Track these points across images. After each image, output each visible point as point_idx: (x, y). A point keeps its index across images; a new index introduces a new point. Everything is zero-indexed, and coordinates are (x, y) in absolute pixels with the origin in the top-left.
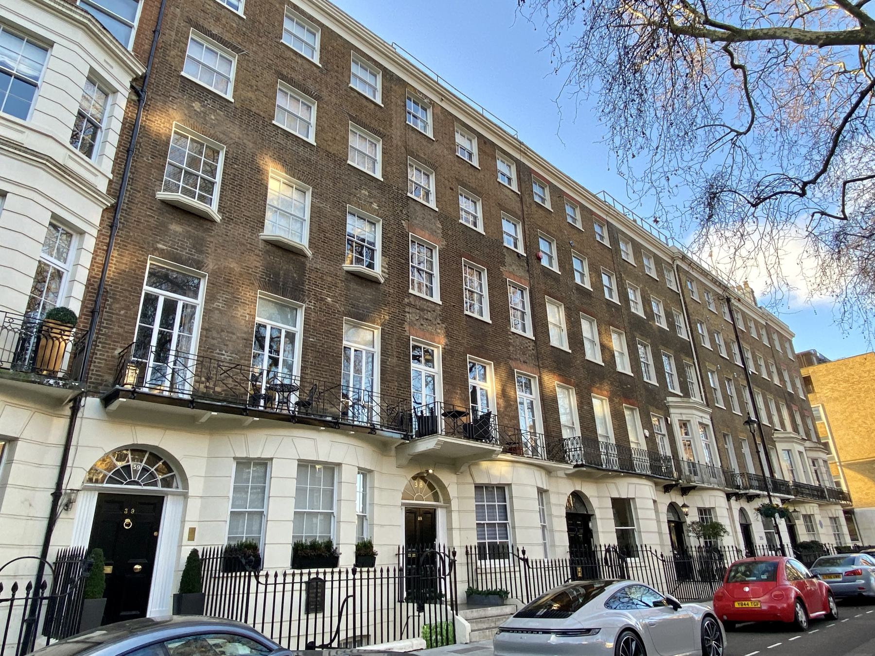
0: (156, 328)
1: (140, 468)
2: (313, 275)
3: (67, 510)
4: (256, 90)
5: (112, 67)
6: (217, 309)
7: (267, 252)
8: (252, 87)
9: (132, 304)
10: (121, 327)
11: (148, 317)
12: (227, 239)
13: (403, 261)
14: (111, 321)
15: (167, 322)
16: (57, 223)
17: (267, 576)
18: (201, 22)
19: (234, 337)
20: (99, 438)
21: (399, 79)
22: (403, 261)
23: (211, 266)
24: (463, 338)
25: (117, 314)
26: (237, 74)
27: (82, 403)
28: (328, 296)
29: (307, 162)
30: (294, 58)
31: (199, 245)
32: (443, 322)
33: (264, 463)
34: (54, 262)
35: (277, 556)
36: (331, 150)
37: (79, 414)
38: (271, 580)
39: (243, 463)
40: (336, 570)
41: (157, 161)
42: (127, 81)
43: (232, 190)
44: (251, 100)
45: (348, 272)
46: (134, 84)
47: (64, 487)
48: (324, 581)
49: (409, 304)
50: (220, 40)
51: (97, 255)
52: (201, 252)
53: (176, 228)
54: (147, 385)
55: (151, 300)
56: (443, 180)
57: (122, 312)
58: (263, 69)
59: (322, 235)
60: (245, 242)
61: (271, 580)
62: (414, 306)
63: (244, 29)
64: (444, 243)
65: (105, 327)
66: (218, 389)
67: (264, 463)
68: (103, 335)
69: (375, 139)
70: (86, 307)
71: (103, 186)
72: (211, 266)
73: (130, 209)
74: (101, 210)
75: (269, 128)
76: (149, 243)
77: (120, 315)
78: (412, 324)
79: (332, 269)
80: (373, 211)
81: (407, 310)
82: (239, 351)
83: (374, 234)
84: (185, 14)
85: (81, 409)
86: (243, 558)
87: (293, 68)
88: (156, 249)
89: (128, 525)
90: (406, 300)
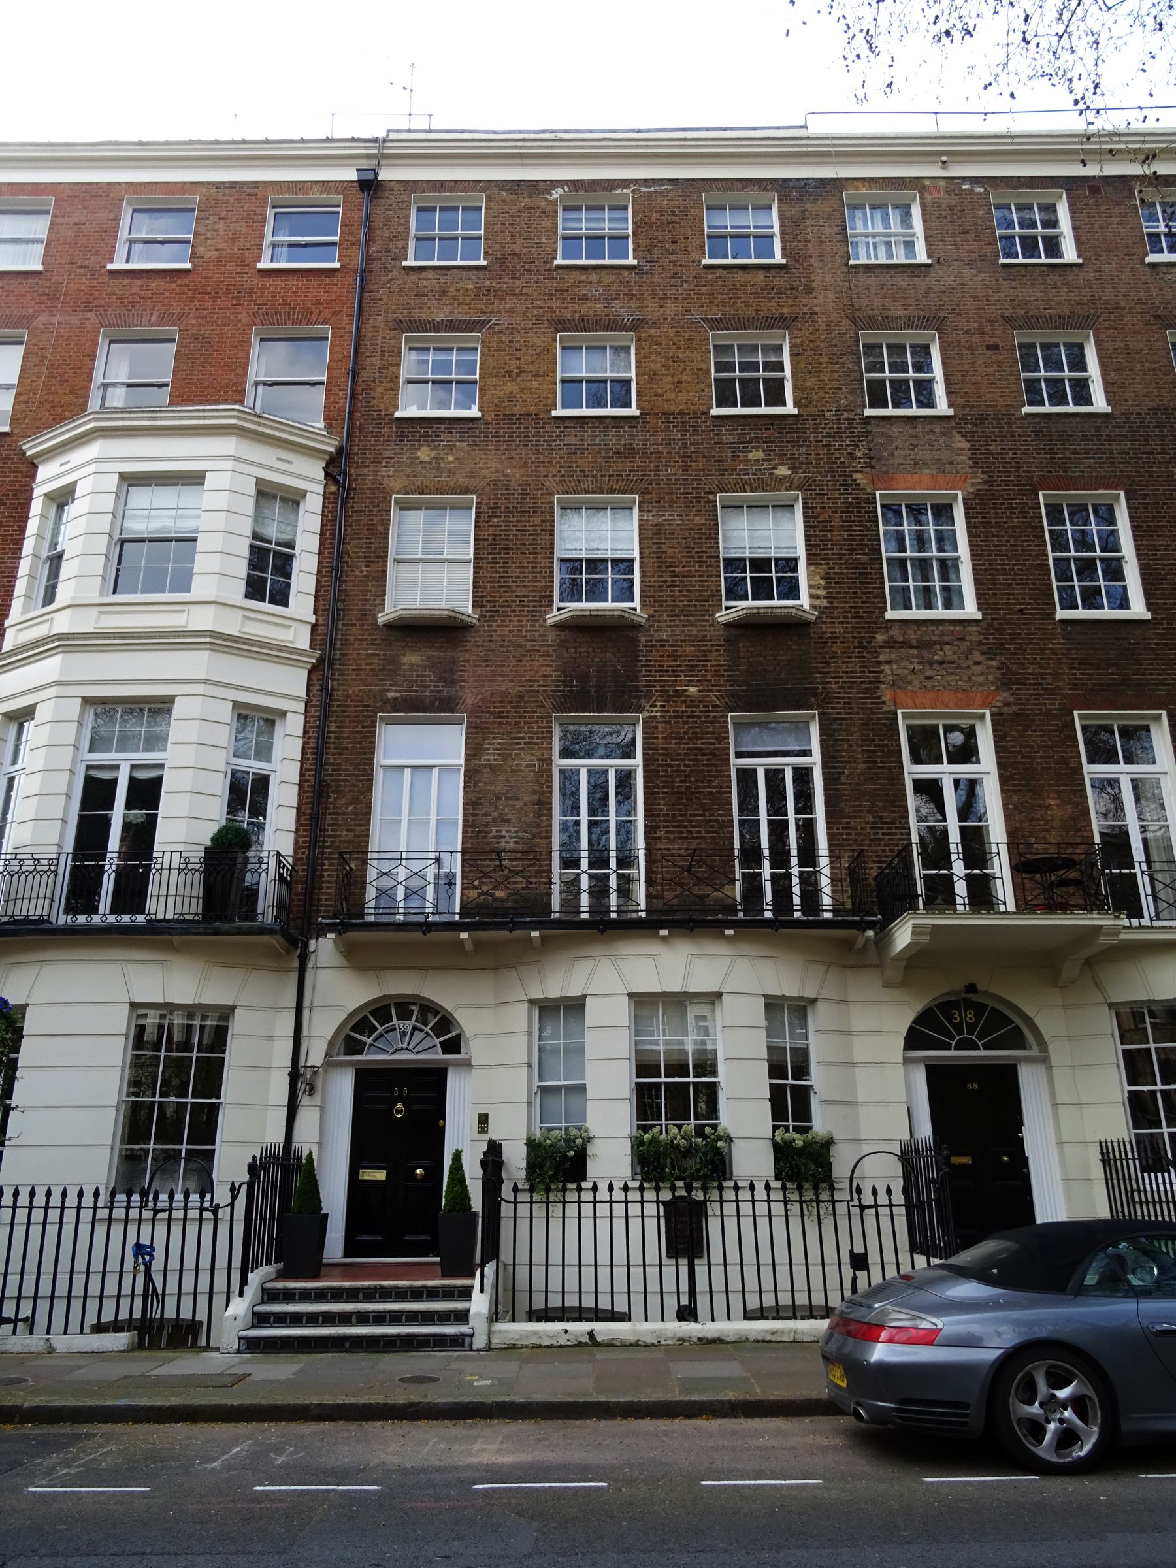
0: (763, 817)
1: (409, 1029)
2: (655, 655)
3: (310, 1095)
4: (518, 375)
5: (290, 462)
6: (485, 766)
7: (563, 644)
8: (509, 373)
9: (362, 793)
10: (351, 831)
11: (748, 804)
12: (493, 646)
13: (865, 558)
14: (339, 825)
15: (598, 804)
16: (244, 714)
17: (595, 1188)
18: (416, 314)
19: (520, 803)
20: (339, 989)
21: (823, 181)
22: (865, 558)
23: (470, 701)
24: (1057, 676)
25: (343, 814)
26: (924, 221)
27: (312, 949)
28: (690, 683)
29: (627, 452)
30: (583, 278)
31: (448, 674)
32: (989, 655)
33: (575, 1006)
34: (253, 765)
35: (611, 1159)
36: (673, 408)
37: (311, 964)
38: (603, 1194)
39: (547, 1009)
40: (729, 1184)
41: (374, 567)
42: (316, 470)
43: (494, 563)
44: (510, 397)
45: (728, 625)
46: (330, 470)
47: (302, 1063)
48: (913, 1250)
49: (890, 644)
50: (452, 326)
51: (310, 738)
52: (452, 683)
53: (411, 659)
54: (401, 910)
55: (569, 777)
56: (964, 338)
57: (350, 809)
58: (528, 330)
59: (666, 576)
60: (521, 640)
61: (603, 1194)
62: (905, 644)
63: (488, 283)
64: (980, 477)
65: (330, 836)
66: (500, 894)
67: (575, 1006)
68: (328, 847)
69: (770, 337)
70: (305, 814)
71: (303, 640)
72: (470, 701)
73: (345, 655)
74: (306, 672)
75: (547, 427)
76: (375, 696)
77: (348, 814)
78: (899, 683)
79: (694, 631)
80: (780, 483)
81: (882, 657)
82: (529, 826)
83: (781, 534)
84: (391, 317)
85: (313, 956)
86: (560, 1166)
87: (584, 299)
88: (387, 701)
89: (398, 1112)
90: (880, 638)
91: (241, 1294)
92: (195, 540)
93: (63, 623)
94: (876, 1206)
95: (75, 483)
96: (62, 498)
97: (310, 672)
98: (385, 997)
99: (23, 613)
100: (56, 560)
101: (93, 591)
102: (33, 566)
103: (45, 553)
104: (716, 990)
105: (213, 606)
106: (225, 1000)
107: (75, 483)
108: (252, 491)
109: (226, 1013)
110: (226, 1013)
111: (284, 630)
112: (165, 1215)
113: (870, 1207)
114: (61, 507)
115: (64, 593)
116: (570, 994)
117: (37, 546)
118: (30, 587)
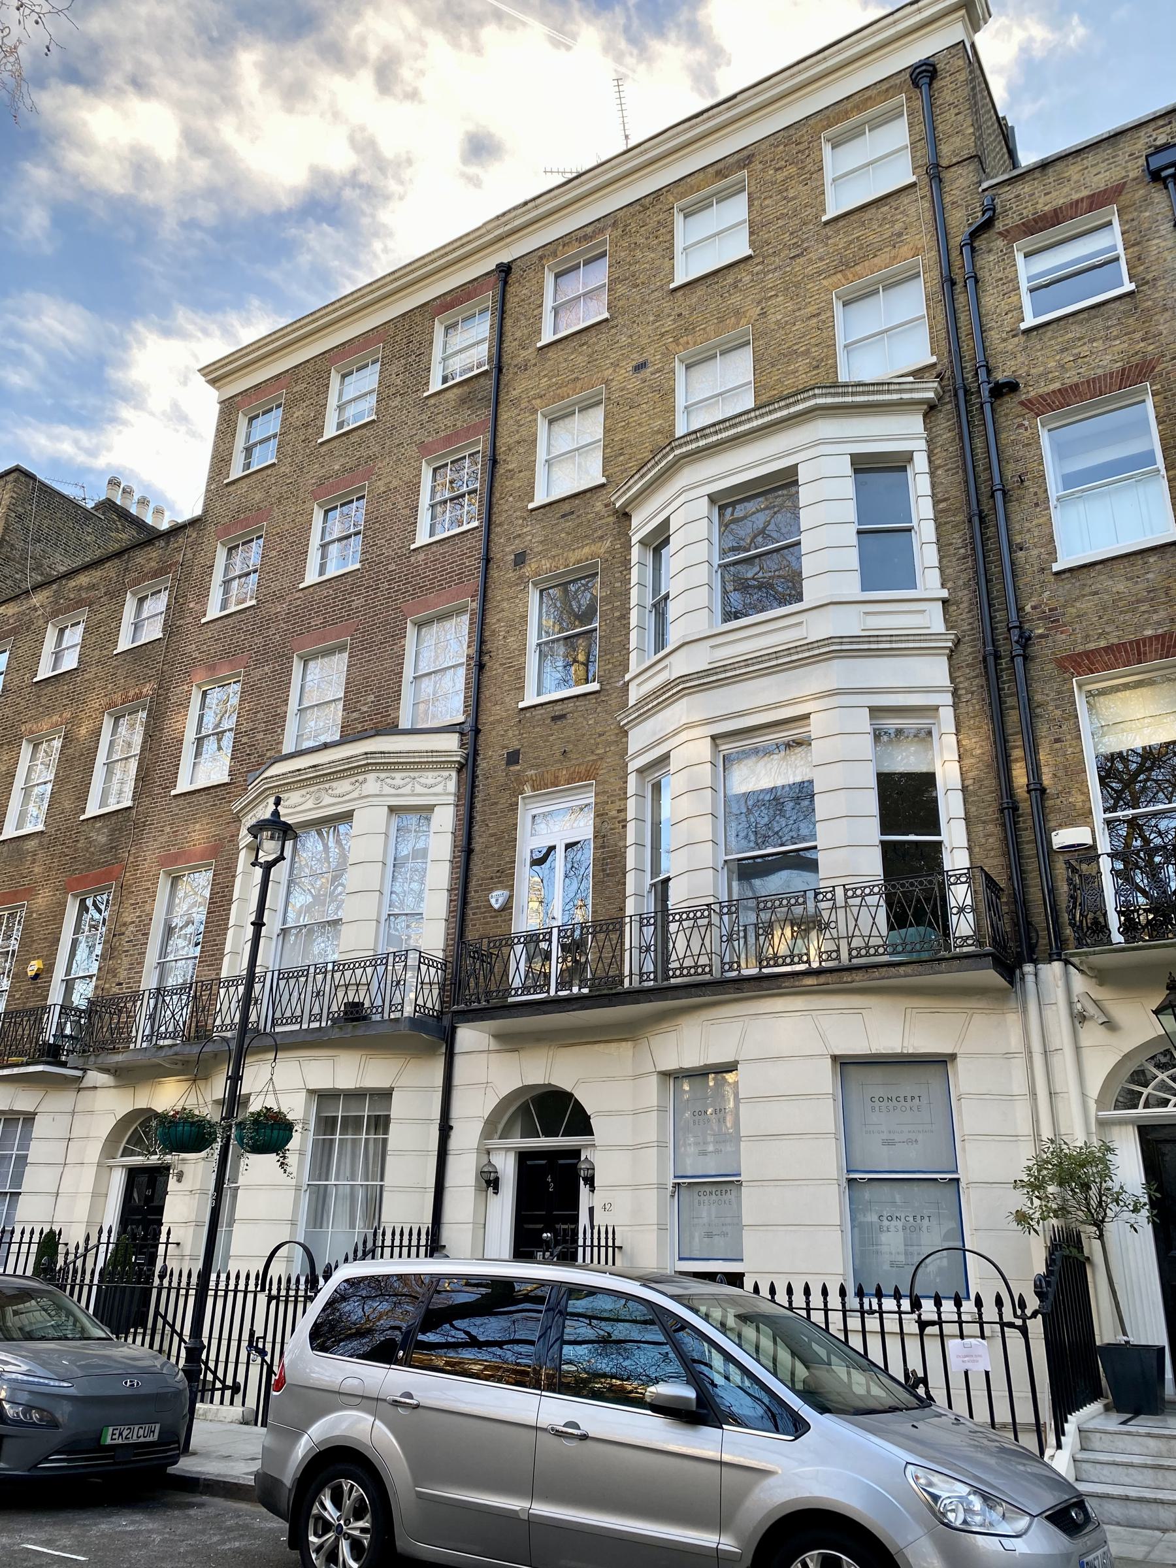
42: (915, 423)
71: (934, 620)
91: (1059, 1446)
92: (798, 543)
93: (680, 665)
94: (940, 1323)
95: (668, 519)
96: (659, 540)
97: (950, 658)
98: (1127, 1057)
99: (638, 665)
100: (660, 607)
101: (701, 624)
102: (641, 617)
103: (649, 601)
104: (950, 1051)
105: (831, 607)
106: (383, 1083)
107: (668, 519)
108: (849, 470)
109: (384, 1095)
110: (384, 1095)
111: (920, 616)
112: (934, 1330)
113: (932, 1323)
114: (657, 551)
115: (674, 635)
116: (686, 1066)
117: (641, 595)
118: (641, 638)
